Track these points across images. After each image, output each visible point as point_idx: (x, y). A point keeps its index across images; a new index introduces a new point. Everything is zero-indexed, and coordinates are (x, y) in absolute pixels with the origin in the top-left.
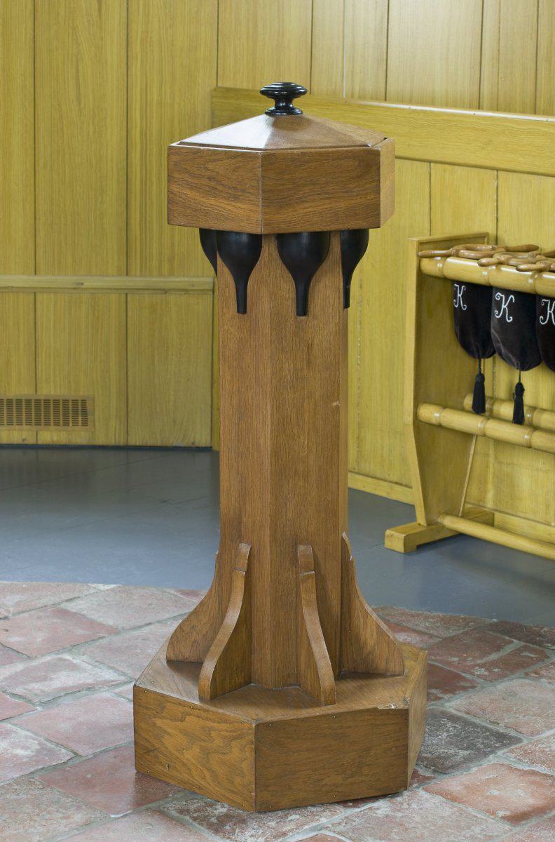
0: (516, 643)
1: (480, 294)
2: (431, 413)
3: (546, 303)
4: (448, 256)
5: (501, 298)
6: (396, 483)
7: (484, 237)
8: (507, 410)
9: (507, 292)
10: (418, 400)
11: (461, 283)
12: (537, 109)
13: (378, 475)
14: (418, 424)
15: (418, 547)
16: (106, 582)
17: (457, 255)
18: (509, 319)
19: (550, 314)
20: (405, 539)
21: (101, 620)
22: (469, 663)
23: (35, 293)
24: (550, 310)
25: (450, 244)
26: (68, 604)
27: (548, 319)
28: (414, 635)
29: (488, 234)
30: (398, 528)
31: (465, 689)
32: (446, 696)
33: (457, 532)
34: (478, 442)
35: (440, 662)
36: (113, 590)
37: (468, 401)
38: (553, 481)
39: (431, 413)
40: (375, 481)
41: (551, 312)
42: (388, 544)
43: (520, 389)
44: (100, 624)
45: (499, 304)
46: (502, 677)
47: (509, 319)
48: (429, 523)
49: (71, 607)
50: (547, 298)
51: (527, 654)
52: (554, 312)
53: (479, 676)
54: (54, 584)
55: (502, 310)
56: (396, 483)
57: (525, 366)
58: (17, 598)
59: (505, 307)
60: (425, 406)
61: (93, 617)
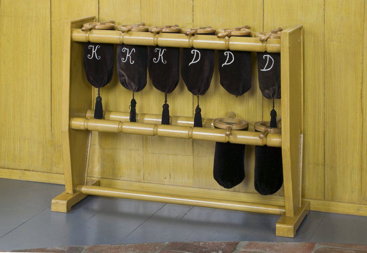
3: (158, 51)
5: (126, 51)
6: (25, 170)
7: (94, 19)
10: (72, 114)
13: (11, 167)
14: (73, 133)
18: (132, 62)
19: (94, 53)
20: (67, 203)
24: (161, 54)
25: (78, 25)
27: (159, 59)
29: (95, 17)
30: (59, 196)
33: (86, 194)
34: (92, 135)
40: (11, 170)
41: (95, 51)
42: (54, 208)
45: (124, 55)
47: (132, 62)
48: (74, 191)
52: (96, 52)
56: (25, 170)
59: (129, 55)
60: (75, 119)
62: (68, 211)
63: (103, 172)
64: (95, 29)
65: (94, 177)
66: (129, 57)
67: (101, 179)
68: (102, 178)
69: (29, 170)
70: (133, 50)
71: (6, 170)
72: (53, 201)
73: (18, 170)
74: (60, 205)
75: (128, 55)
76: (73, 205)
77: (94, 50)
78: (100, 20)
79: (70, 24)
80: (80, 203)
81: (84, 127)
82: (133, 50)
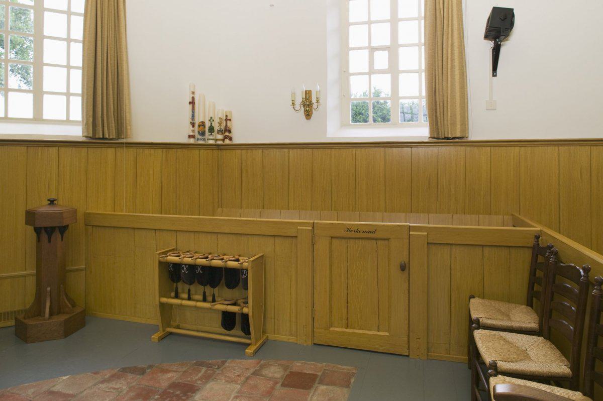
0: (204, 369)
1: (177, 266)
2: (164, 300)
4: (167, 256)
8: (185, 296)
9: (186, 265)
10: (161, 296)
11: (171, 263)
12: (115, 209)
15: (161, 339)
16: (65, 376)
17: (170, 256)
21: (67, 392)
22: (194, 379)
23: (408, 356)
26: (53, 388)
28: (174, 373)
31: (198, 390)
32: (194, 395)
35: (186, 381)
36: (68, 378)
37: (173, 294)
38: (571, 398)
39: (164, 300)
43: (189, 290)
44: (68, 394)
46: (207, 382)
49: (55, 389)
50: (184, 265)
51: (209, 372)
53: (200, 384)
54: (46, 381)
55: (184, 270)
57: (191, 284)
58: (32, 390)
61: (64, 392)
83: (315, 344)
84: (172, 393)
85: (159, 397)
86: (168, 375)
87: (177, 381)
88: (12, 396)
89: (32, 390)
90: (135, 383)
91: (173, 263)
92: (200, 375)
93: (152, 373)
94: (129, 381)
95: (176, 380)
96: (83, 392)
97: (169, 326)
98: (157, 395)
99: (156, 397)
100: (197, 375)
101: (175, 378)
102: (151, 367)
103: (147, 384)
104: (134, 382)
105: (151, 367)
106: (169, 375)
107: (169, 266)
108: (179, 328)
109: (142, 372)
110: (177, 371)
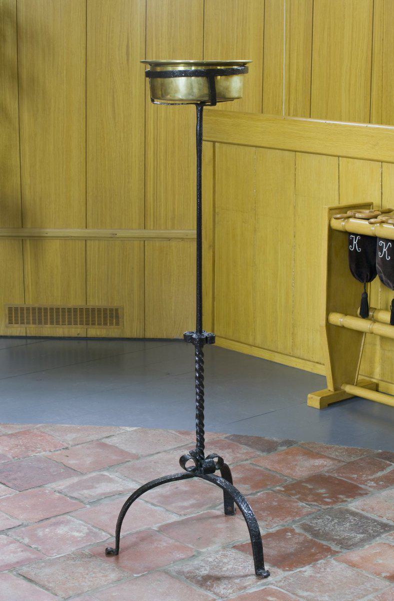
1: (368, 241)
2: (337, 319)
5: (383, 244)
6: (317, 363)
7: (370, 205)
9: (387, 240)
10: (330, 308)
11: (356, 235)
15: (328, 404)
19: (355, 244)
21: (127, 450)
25: (346, 211)
26: (107, 439)
31: (361, 495)
32: (349, 500)
33: (349, 394)
35: (345, 477)
36: (135, 431)
39: (337, 319)
40: (304, 361)
41: (356, 243)
45: (381, 249)
47: (388, 258)
48: (336, 389)
56: (317, 363)
58: (74, 436)
59: (385, 250)
62: (323, 407)
63: (383, 374)
64: (355, 218)
65: (374, 378)
66: (385, 251)
67: (380, 382)
68: (382, 380)
69: (320, 364)
70: (390, 245)
71: (300, 360)
72: (309, 396)
73: (310, 361)
74: (314, 401)
75: (384, 250)
76: (330, 402)
77: (355, 241)
78: (21, 242)
79: (327, 210)
80: (339, 402)
81: (341, 324)
82: (390, 245)
83: (22, 227)
84: (311, 489)
85: (283, 489)
86: (317, 461)
87: (327, 474)
88: (41, 436)
89: (74, 436)
90: (248, 462)
91: (361, 235)
92: (380, 474)
93: (287, 453)
94: (238, 455)
95: (327, 472)
96: (153, 455)
97: (351, 382)
98: (280, 486)
99: (278, 488)
100: (374, 472)
101: (326, 469)
102: (288, 443)
103: (269, 467)
104: (247, 460)
105: (288, 443)
106: (318, 462)
107: (351, 243)
108: (377, 390)
109: (270, 447)
110: (335, 459)
